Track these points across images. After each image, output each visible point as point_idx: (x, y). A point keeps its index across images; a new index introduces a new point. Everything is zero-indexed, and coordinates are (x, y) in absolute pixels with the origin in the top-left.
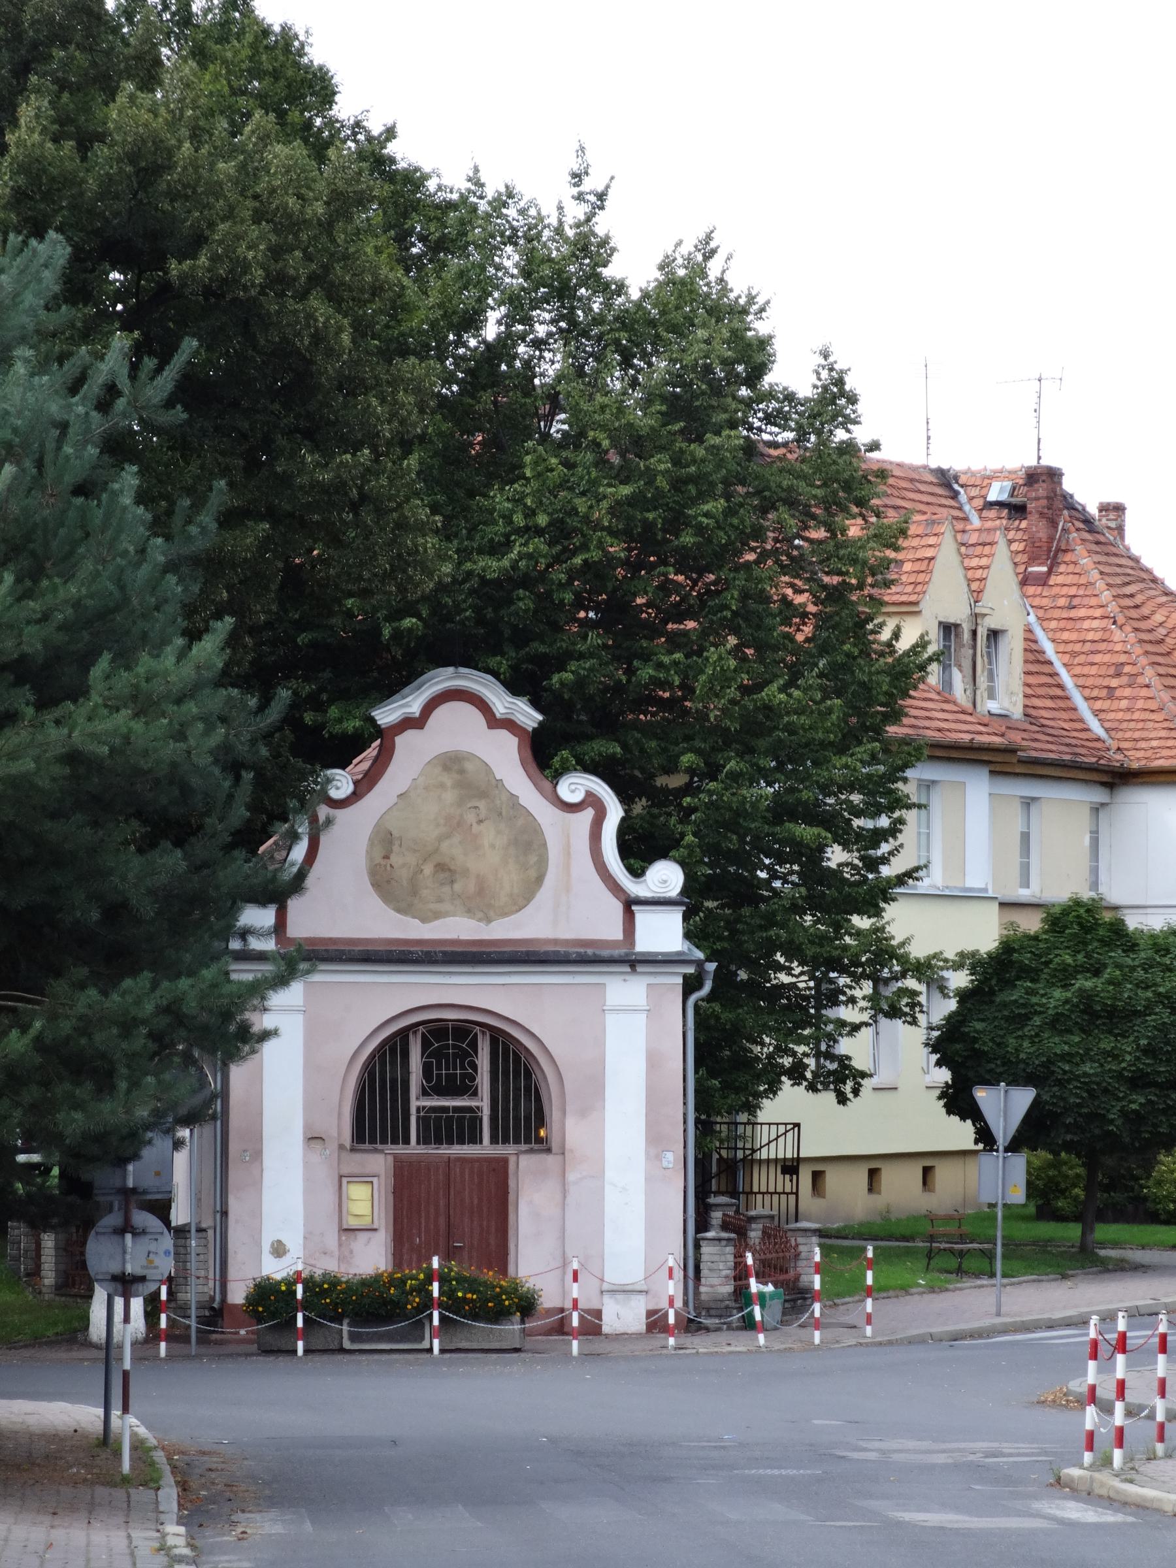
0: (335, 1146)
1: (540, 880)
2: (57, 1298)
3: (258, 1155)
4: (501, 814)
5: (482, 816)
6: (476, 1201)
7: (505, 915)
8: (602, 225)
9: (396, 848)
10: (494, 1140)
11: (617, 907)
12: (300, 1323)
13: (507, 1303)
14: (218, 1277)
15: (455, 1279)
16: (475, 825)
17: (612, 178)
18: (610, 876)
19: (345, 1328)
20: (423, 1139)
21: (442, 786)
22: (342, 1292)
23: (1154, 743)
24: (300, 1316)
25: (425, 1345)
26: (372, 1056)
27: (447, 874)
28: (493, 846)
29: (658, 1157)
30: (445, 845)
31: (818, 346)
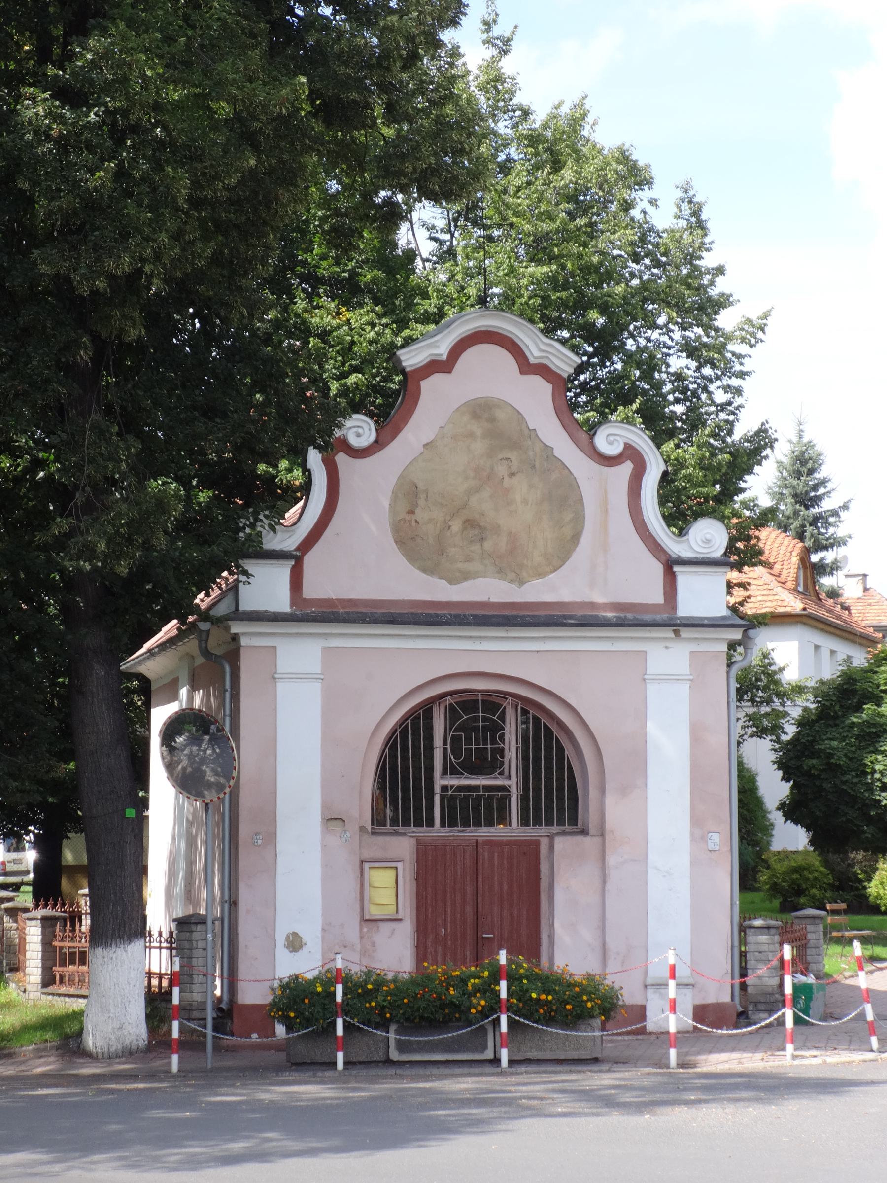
0: (357, 828)
1: (576, 538)
2: (44, 997)
3: (271, 838)
4: (534, 467)
5: (514, 469)
6: (505, 888)
7: (541, 575)
8: (507, 66)
9: (421, 502)
10: (525, 822)
11: (658, 569)
12: (340, 1031)
13: (589, 1005)
14: (225, 975)
15: (527, 977)
16: (506, 478)
17: (516, 27)
18: (650, 535)
19: (392, 1036)
20: (449, 820)
21: (471, 435)
22: (389, 993)
23: (760, 598)
24: (340, 1022)
25: (489, 1054)
26: (394, 732)
27: (476, 531)
28: (525, 502)
29: (704, 839)
30: (474, 500)
31: (681, 181)
